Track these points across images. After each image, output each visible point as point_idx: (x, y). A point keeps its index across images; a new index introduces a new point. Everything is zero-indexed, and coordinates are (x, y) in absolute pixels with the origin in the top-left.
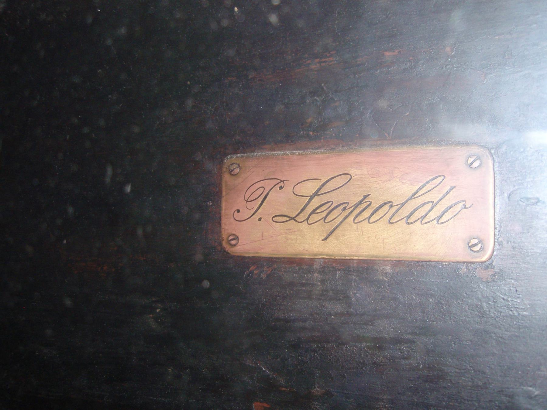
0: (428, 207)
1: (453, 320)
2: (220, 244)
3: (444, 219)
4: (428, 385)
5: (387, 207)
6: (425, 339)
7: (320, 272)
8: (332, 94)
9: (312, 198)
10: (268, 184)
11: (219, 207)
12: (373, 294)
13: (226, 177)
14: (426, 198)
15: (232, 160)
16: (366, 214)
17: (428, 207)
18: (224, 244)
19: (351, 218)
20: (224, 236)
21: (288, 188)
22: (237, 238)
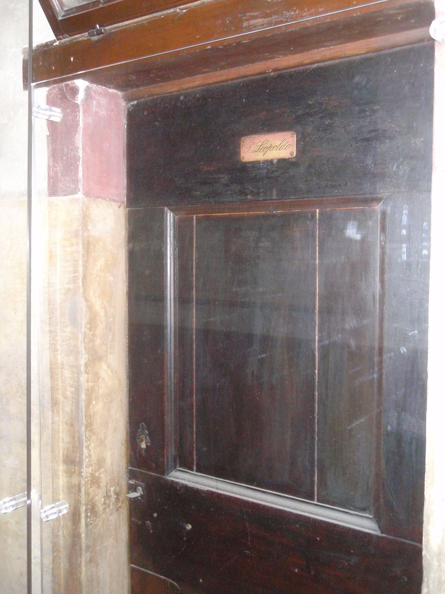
0: (283, 146)
1: (53, 168)
2: (240, 159)
3: (286, 148)
4: (329, 123)
5: (275, 147)
6: (206, 205)
7: (262, 163)
8: (399, 442)
9: (260, 146)
10: (251, 144)
11: (240, 150)
12: (392, 190)
13: (242, 143)
14: (283, 144)
15: (243, 138)
16: (271, 149)
17: (283, 146)
18: (241, 159)
19: (268, 150)
20: (241, 157)
21: (255, 144)
22: (244, 157)
